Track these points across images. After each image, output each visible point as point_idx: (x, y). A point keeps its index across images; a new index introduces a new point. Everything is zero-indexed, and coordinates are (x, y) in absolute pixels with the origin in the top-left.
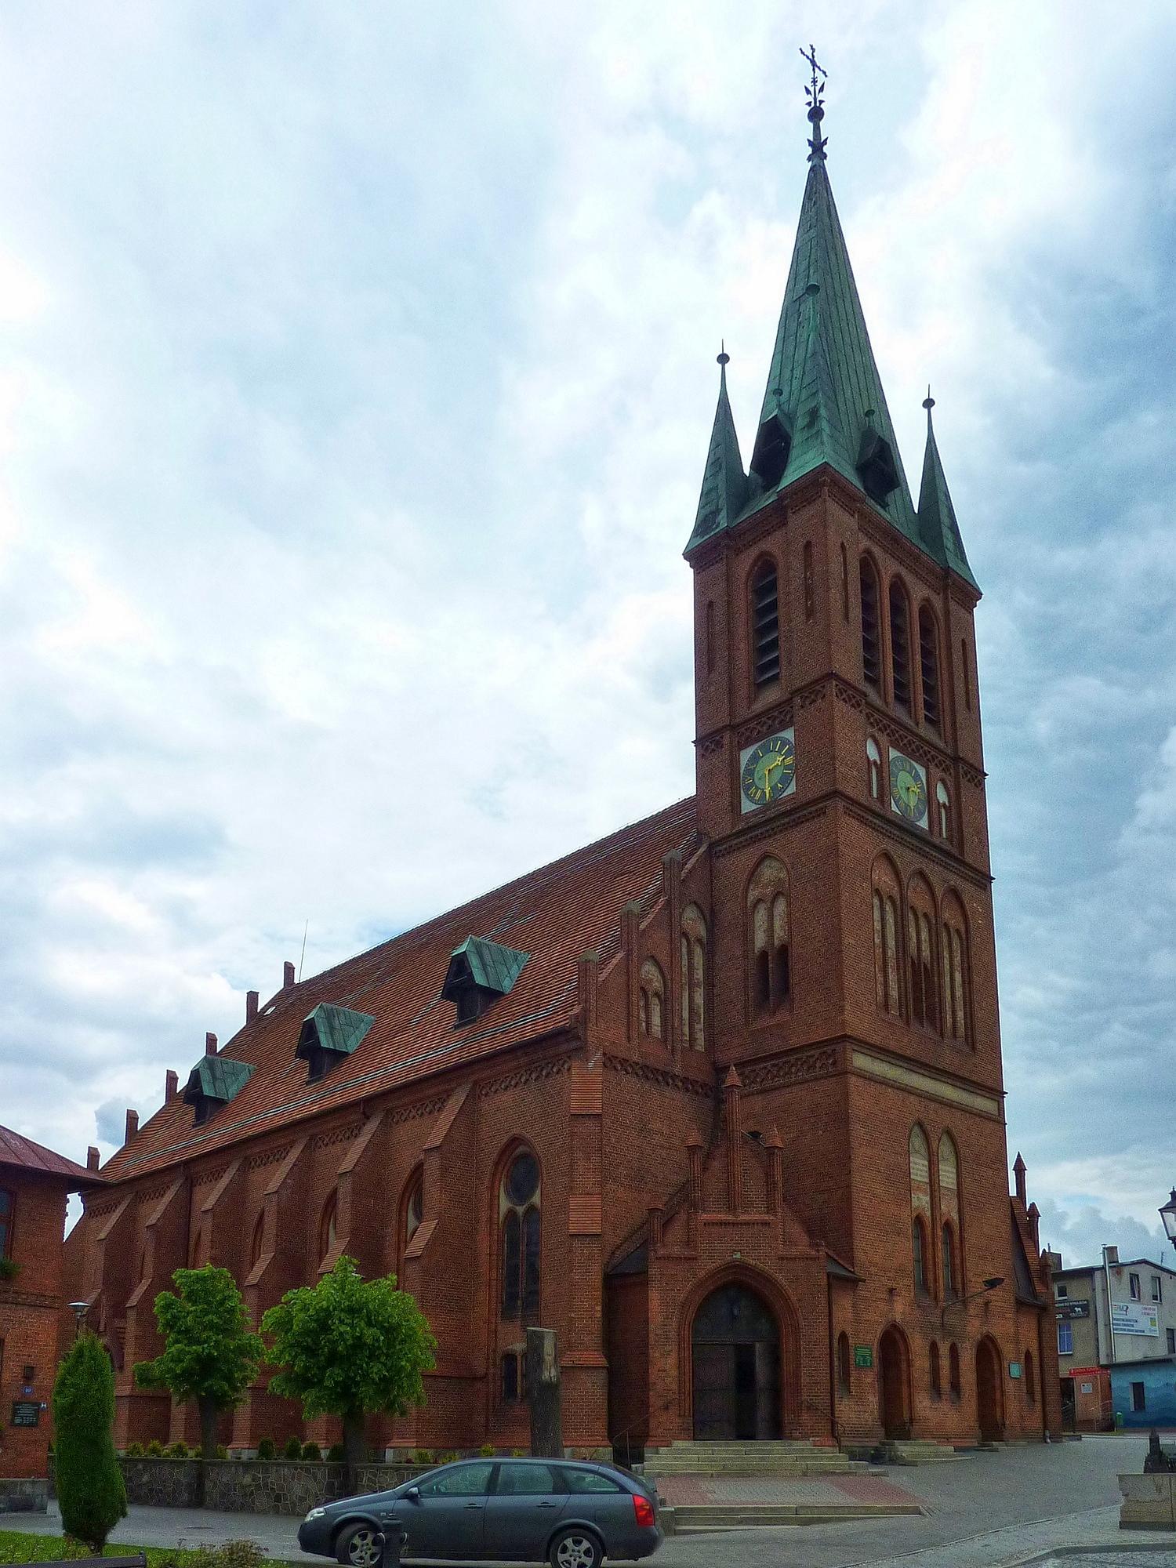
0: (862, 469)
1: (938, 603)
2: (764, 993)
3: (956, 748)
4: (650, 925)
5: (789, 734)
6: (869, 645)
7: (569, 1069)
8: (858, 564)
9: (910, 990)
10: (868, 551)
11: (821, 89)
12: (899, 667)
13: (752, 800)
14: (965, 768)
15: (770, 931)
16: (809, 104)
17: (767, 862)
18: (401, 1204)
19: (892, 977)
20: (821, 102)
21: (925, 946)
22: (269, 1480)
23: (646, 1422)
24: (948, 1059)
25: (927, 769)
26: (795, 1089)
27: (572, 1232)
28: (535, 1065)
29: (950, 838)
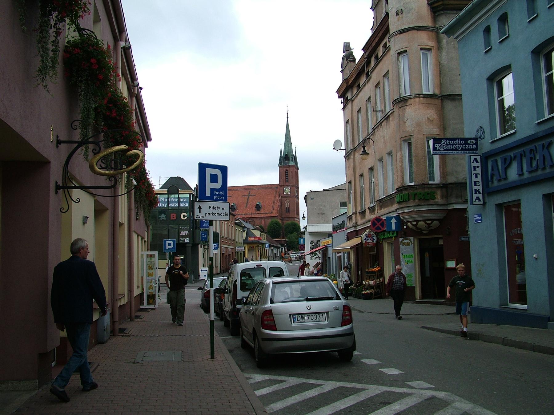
5: (290, 188)
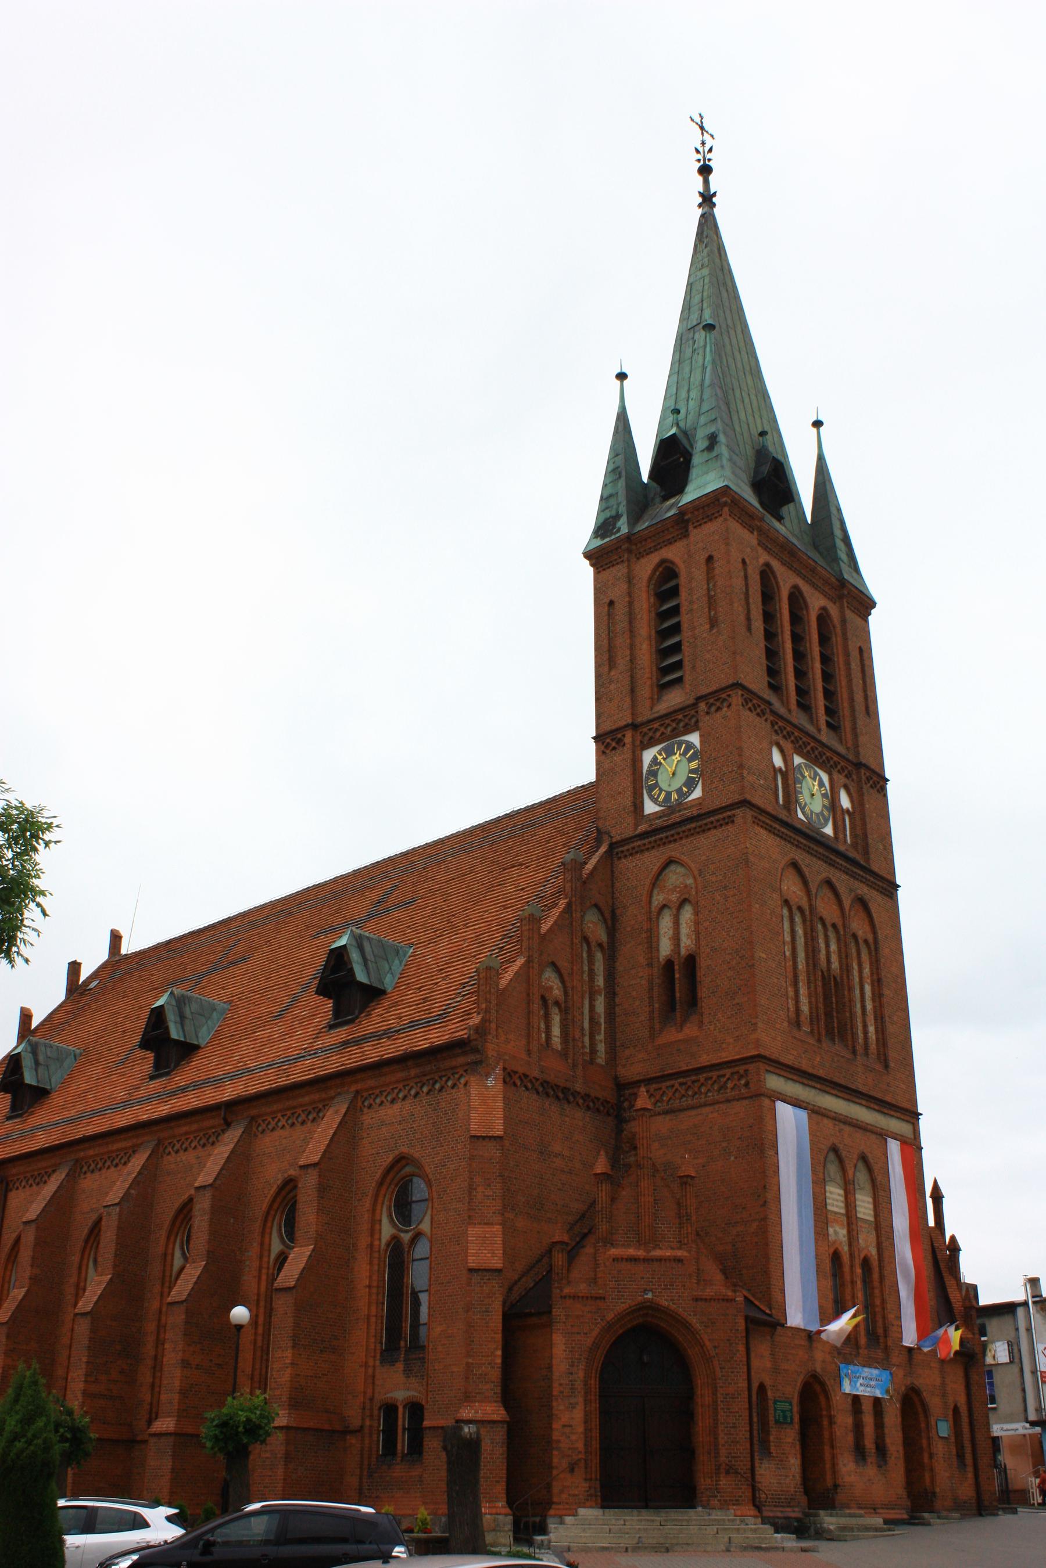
0: (758, 486)
1: (834, 611)
2: (670, 1005)
3: (857, 754)
4: (551, 930)
5: (694, 738)
6: (772, 655)
7: (465, 1085)
8: (758, 577)
9: (821, 1006)
10: (767, 565)
11: (710, 150)
12: (800, 674)
13: (655, 800)
14: (868, 774)
15: (676, 939)
16: (699, 161)
17: (673, 867)
18: (266, 1221)
19: (803, 991)
20: (709, 160)
21: (834, 958)
23: (549, 1487)
24: (862, 1082)
25: (830, 774)
26: (705, 1110)
27: (472, 1265)
28: (428, 1077)
29: (854, 845)
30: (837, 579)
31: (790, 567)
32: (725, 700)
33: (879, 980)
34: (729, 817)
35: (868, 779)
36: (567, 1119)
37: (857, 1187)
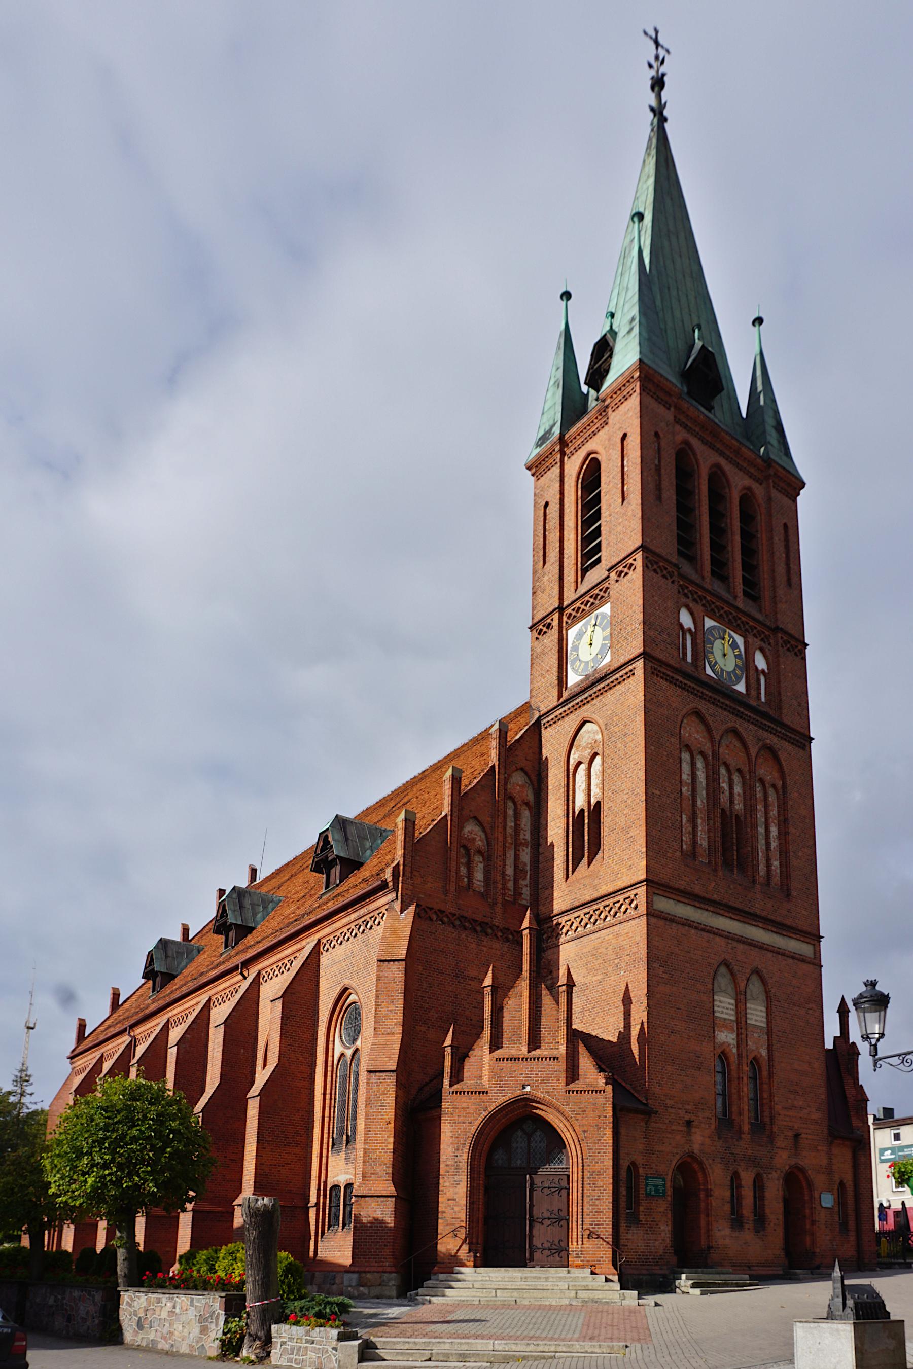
0: (686, 375)
1: (759, 491)
10: (686, 442)
22: (65, 1301)
24: (759, 905)
25: (745, 637)
30: (763, 460)
31: (712, 447)
32: (632, 565)
33: (786, 820)
34: (631, 671)
35: (786, 642)
36: (485, 949)
37: (748, 997)
